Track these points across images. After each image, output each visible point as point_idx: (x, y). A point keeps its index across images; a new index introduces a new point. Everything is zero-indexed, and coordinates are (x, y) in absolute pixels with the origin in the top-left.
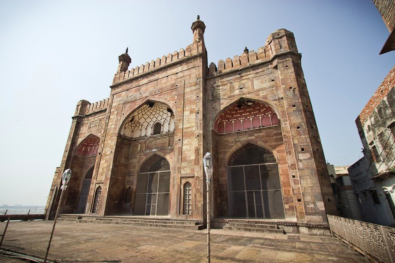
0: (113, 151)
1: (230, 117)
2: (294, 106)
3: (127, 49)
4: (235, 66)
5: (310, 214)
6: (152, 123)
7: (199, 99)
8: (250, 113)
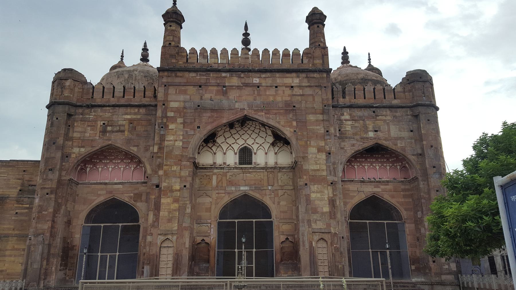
2: (434, 167)
4: (369, 99)
6: (236, 147)
7: (329, 135)
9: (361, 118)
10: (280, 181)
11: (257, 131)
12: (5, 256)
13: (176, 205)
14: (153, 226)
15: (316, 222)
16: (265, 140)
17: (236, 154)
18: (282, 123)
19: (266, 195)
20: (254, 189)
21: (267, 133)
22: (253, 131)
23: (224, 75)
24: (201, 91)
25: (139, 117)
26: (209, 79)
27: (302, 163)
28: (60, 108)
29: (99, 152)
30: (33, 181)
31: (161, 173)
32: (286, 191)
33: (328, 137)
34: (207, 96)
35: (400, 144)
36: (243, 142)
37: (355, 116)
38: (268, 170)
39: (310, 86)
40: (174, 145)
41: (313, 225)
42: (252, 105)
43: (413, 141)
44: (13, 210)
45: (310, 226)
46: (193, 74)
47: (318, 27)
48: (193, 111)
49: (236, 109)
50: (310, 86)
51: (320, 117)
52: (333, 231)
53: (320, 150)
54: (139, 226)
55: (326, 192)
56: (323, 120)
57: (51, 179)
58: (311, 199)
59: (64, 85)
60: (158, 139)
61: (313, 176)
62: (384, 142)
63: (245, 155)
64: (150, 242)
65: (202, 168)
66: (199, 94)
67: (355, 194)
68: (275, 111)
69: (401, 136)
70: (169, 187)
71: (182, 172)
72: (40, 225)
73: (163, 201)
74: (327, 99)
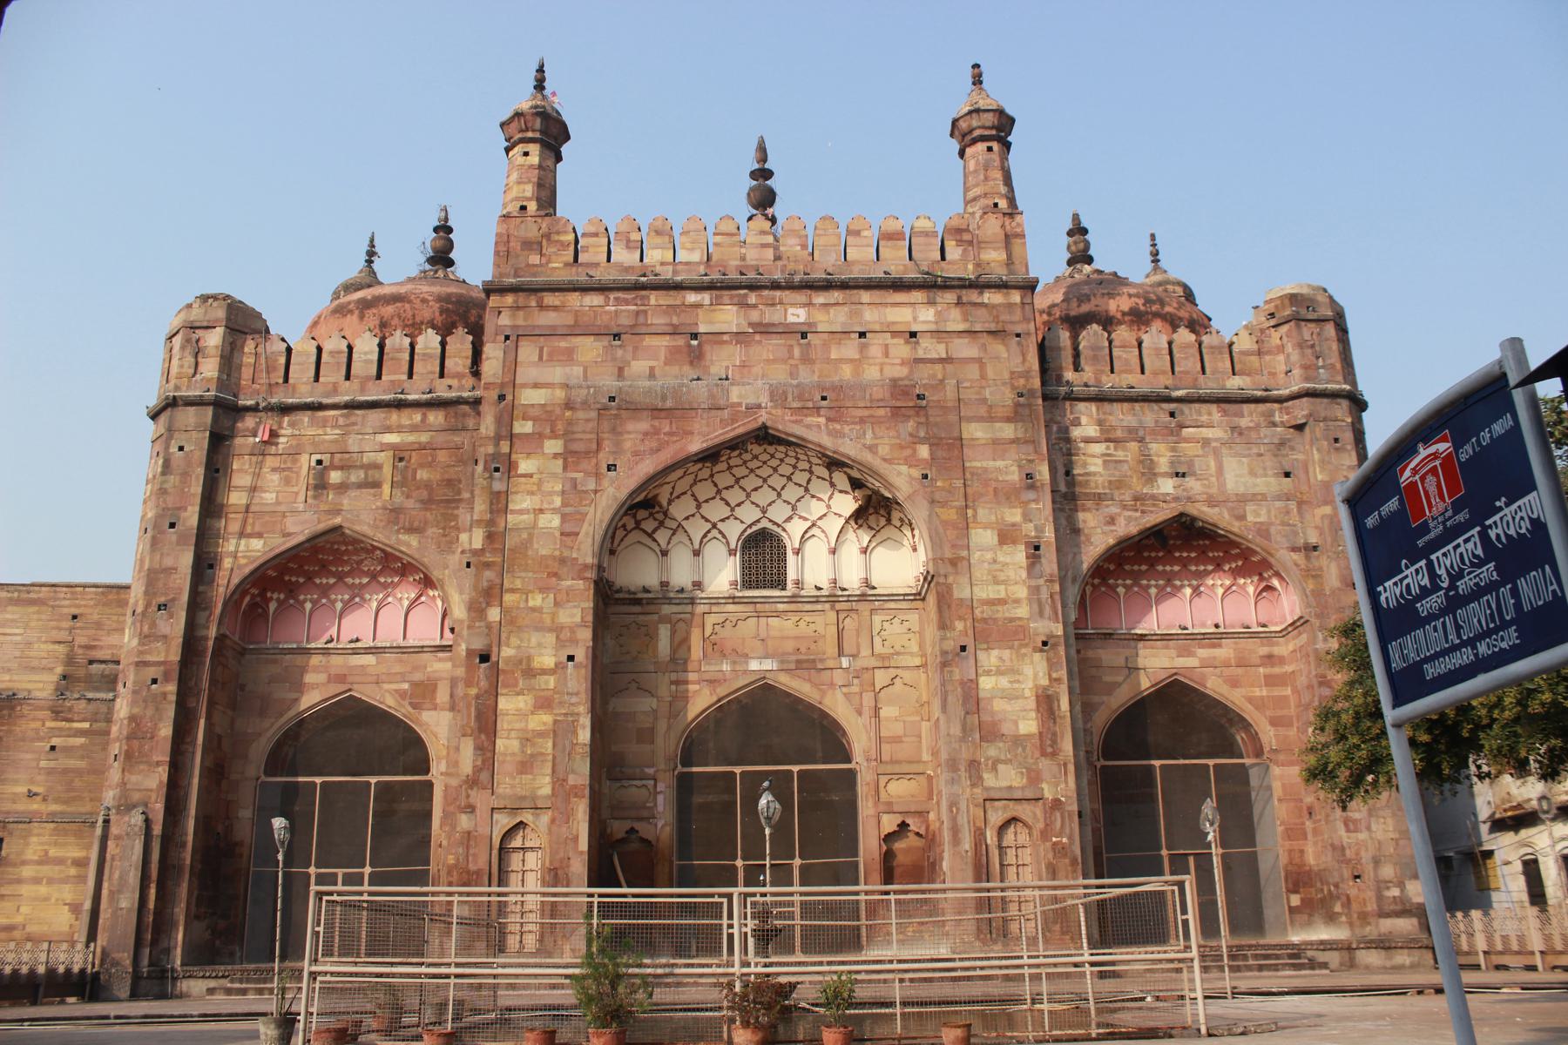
0: (581, 654)
1: (1112, 567)
3: (541, 70)
4: (1155, 374)
5: (1388, 915)
6: (734, 531)
7: (1032, 487)
8: (1185, 566)
9: (1136, 435)
10: (877, 640)
11: (801, 477)
12: (19, 881)
13: (543, 720)
14: (472, 782)
15: (994, 769)
16: (829, 507)
19: (832, 685)
21: (832, 485)
22: (789, 478)
23: (692, 297)
24: (620, 352)
25: (424, 438)
26: (645, 312)
27: (950, 579)
28: (189, 416)
29: (306, 550)
30: (101, 648)
31: (494, 614)
32: (899, 672)
33: (1031, 495)
34: (639, 366)
35: (1256, 515)
36: (757, 514)
37: (1113, 428)
38: (838, 607)
39: (970, 333)
41: (985, 776)
42: (785, 393)
43: (1293, 505)
44: (41, 739)
45: (977, 780)
46: (594, 300)
47: (990, 149)
49: (733, 405)
50: (970, 333)
51: (1008, 431)
53: (1006, 536)
54: (430, 785)
55: (1028, 671)
57: (165, 637)
58: (981, 695)
59: (201, 344)
60: (483, 507)
61: (985, 620)
62: (1205, 509)
64: (469, 833)
65: (623, 602)
66: (614, 359)
67: (1120, 679)
68: (860, 413)
69: (1257, 490)
70: (520, 662)
72: (134, 778)
73: (504, 704)
74: (1026, 375)
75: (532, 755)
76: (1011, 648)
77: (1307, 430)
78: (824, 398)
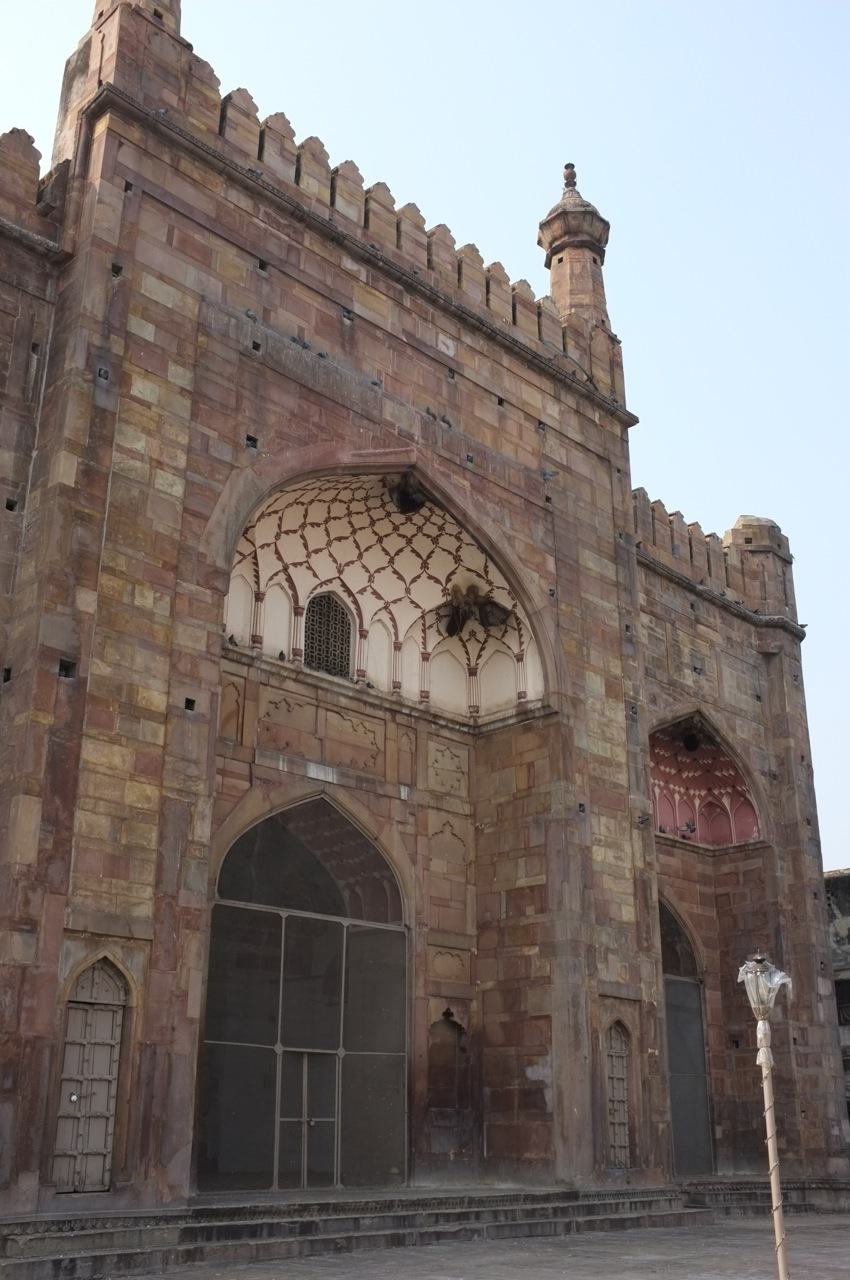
10: (431, 772)
13: (142, 794)
15: (606, 959)
16: (408, 591)
17: (297, 611)
18: (520, 547)
20: (352, 783)
21: (425, 566)
23: (349, 264)
27: (572, 721)
33: (628, 649)
40: (150, 484)
41: (599, 966)
48: (233, 356)
52: (645, 998)
53: (612, 689)
55: (628, 849)
56: (617, 584)
63: (329, 624)
64: (24, 969)
70: (119, 689)
71: (180, 629)
73: (93, 752)
75: (129, 848)
76: (615, 818)
77: (776, 660)
78: (470, 459)
